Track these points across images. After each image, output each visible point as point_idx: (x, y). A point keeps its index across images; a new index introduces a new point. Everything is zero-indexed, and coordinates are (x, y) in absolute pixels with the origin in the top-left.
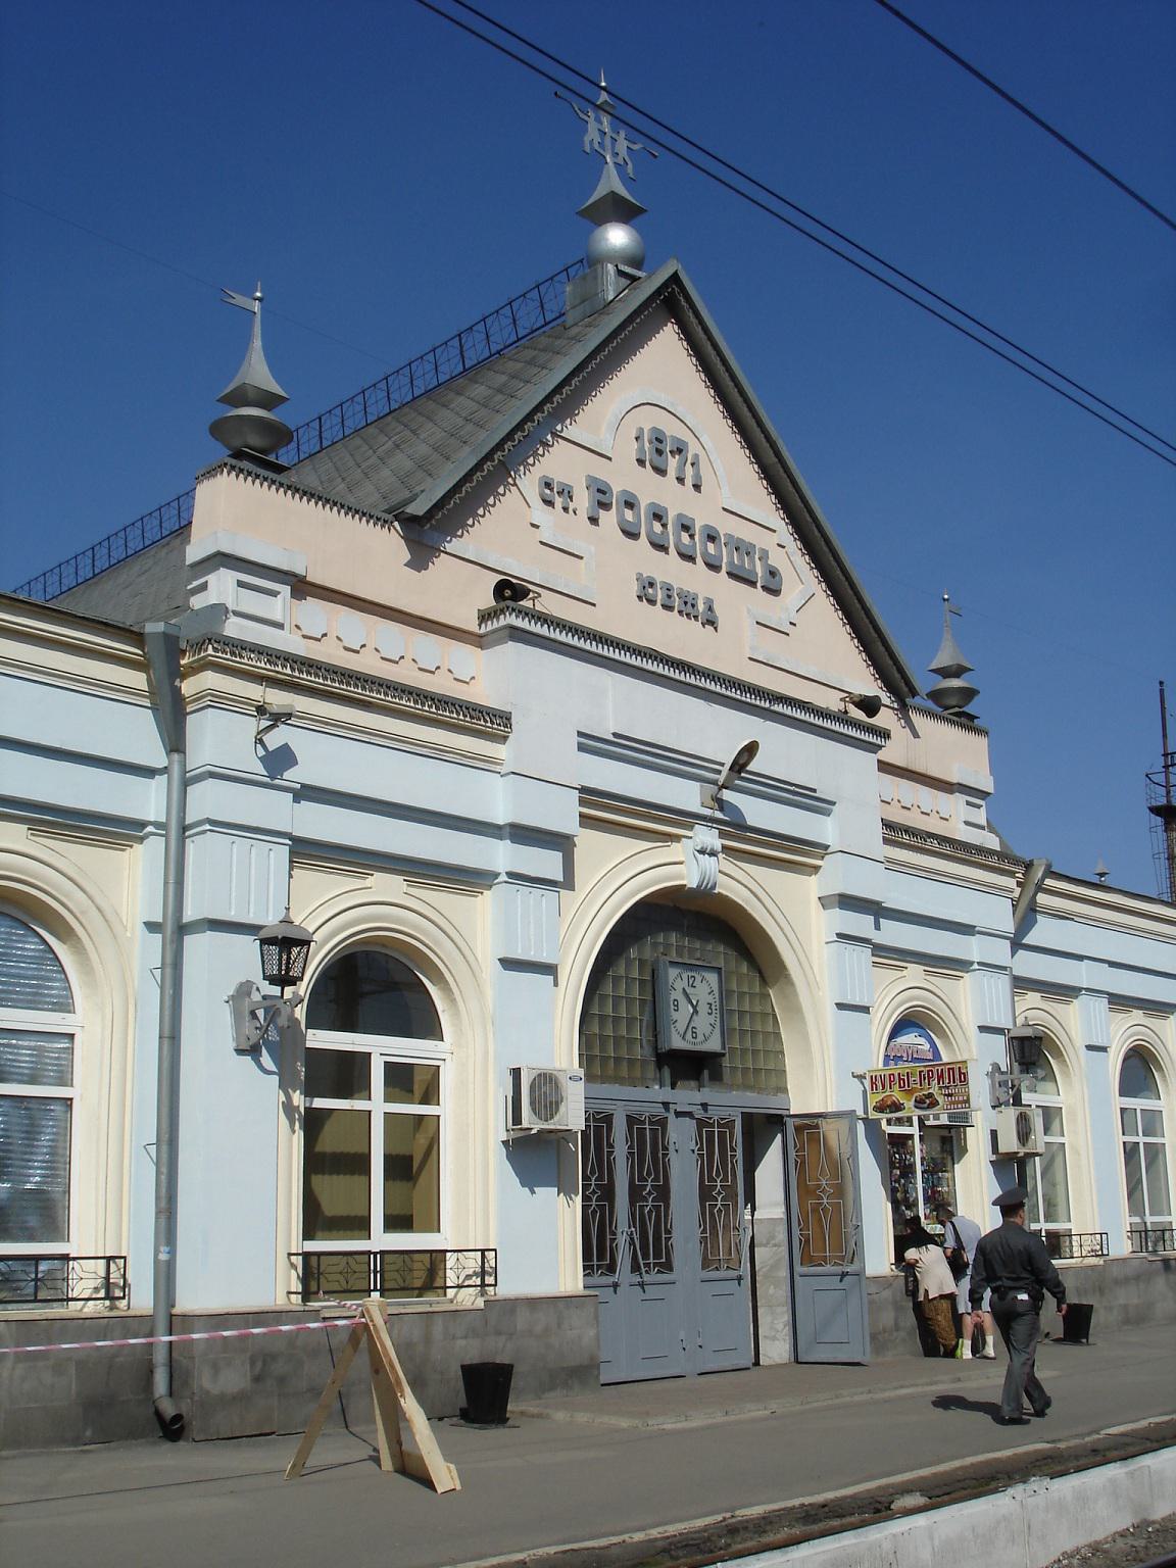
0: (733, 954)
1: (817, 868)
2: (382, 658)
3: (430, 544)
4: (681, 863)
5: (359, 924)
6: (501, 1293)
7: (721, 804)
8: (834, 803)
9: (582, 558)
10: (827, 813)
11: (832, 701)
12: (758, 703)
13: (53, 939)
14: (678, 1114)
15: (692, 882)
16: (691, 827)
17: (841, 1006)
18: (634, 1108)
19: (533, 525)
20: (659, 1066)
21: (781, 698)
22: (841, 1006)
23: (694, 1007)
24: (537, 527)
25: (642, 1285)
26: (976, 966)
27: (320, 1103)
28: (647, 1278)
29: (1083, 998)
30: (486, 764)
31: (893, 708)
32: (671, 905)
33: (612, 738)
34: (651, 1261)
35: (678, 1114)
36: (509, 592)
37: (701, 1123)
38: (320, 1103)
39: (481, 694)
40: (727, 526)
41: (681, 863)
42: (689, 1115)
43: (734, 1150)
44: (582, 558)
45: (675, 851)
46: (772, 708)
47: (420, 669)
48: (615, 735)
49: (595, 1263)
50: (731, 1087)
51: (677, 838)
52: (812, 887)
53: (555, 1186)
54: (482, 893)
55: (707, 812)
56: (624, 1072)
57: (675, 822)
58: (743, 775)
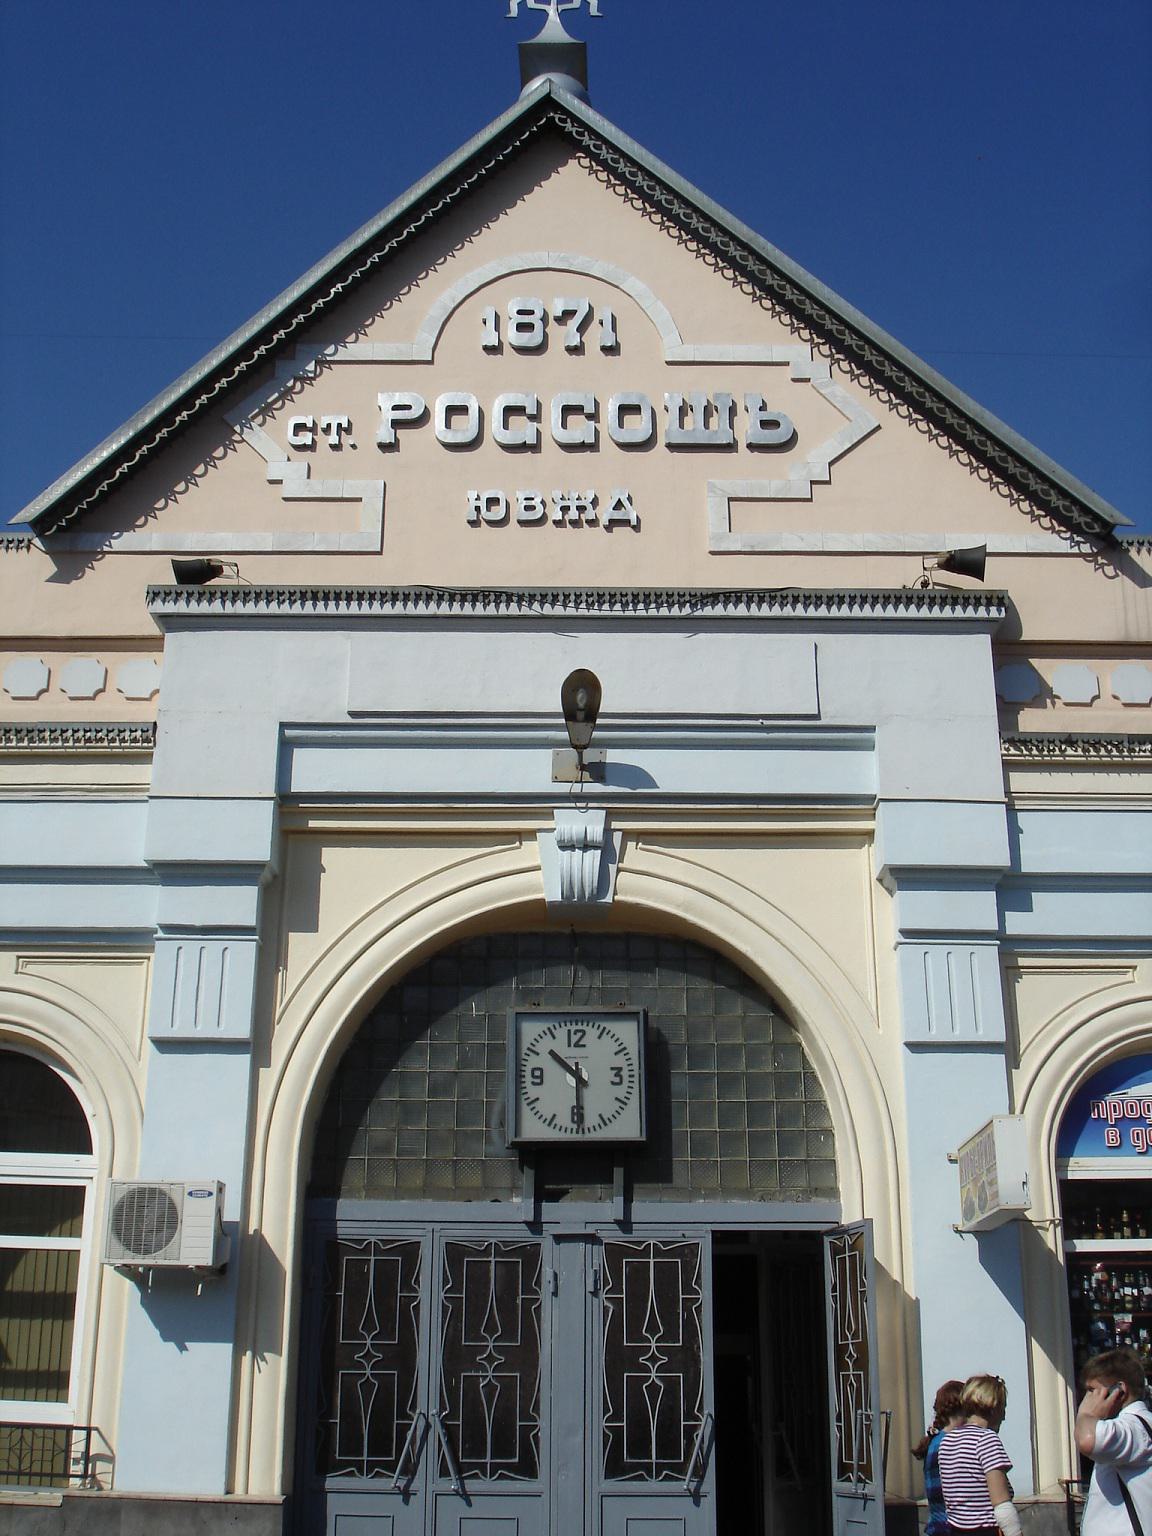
0: (702, 985)
1: (870, 835)
2: (14, 698)
3: (87, 549)
4: (537, 868)
5: (1102, 1038)
6: (117, 1489)
7: (598, 772)
8: (872, 729)
9: (360, 500)
10: (869, 746)
11: (905, 575)
12: (653, 612)
13: (68, 1076)
14: (559, 1239)
15: (553, 894)
16: (548, 815)
17: (915, 1047)
18: (458, 1234)
19: (272, 482)
20: (523, 1163)
21: (713, 595)
22: (915, 1047)
23: (576, 1074)
24: (280, 482)
25: (466, 1497)
26: (160, 934)
27: (1084, 1245)
28: (471, 1485)
29: (164, 949)
30: (127, 794)
31: (1080, 555)
32: (567, 931)
33: (350, 720)
34: (488, 1460)
35: (559, 1239)
36: (195, 573)
37: (614, 1253)
38: (1084, 1245)
39: (110, 710)
40: (702, 387)
41: (537, 868)
42: (592, 1239)
43: (834, 1297)
44: (360, 500)
45: (527, 853)
46: (695, 614)
47: (72, 699)
48: (353, 714)
49: (365, 1458)
50: (692, 1193)
51: (531, 835)
52: (866, 862)
53: (230, 1342)
54: (148, 958)
55: (564, 788)
56: (476, 1180)
57: (653, 814)
58: (599, 721)
